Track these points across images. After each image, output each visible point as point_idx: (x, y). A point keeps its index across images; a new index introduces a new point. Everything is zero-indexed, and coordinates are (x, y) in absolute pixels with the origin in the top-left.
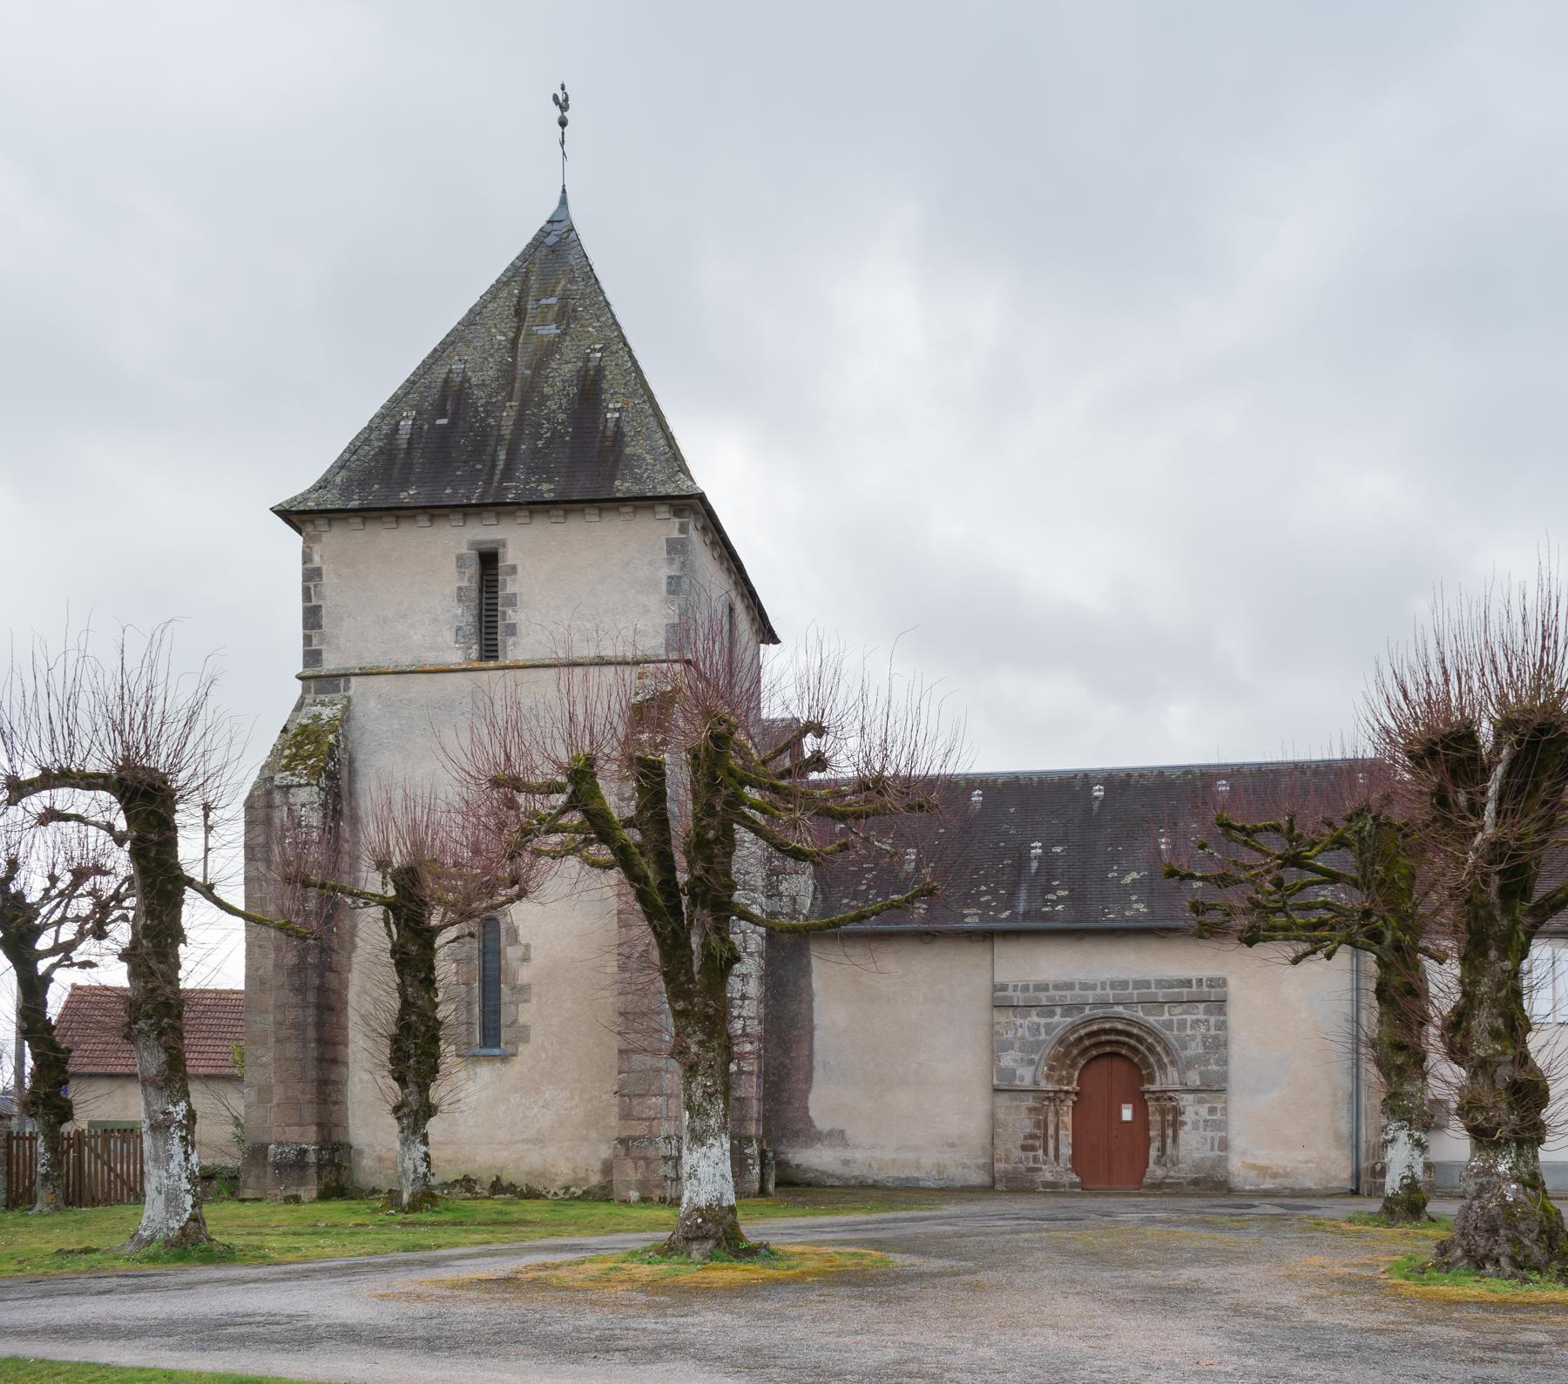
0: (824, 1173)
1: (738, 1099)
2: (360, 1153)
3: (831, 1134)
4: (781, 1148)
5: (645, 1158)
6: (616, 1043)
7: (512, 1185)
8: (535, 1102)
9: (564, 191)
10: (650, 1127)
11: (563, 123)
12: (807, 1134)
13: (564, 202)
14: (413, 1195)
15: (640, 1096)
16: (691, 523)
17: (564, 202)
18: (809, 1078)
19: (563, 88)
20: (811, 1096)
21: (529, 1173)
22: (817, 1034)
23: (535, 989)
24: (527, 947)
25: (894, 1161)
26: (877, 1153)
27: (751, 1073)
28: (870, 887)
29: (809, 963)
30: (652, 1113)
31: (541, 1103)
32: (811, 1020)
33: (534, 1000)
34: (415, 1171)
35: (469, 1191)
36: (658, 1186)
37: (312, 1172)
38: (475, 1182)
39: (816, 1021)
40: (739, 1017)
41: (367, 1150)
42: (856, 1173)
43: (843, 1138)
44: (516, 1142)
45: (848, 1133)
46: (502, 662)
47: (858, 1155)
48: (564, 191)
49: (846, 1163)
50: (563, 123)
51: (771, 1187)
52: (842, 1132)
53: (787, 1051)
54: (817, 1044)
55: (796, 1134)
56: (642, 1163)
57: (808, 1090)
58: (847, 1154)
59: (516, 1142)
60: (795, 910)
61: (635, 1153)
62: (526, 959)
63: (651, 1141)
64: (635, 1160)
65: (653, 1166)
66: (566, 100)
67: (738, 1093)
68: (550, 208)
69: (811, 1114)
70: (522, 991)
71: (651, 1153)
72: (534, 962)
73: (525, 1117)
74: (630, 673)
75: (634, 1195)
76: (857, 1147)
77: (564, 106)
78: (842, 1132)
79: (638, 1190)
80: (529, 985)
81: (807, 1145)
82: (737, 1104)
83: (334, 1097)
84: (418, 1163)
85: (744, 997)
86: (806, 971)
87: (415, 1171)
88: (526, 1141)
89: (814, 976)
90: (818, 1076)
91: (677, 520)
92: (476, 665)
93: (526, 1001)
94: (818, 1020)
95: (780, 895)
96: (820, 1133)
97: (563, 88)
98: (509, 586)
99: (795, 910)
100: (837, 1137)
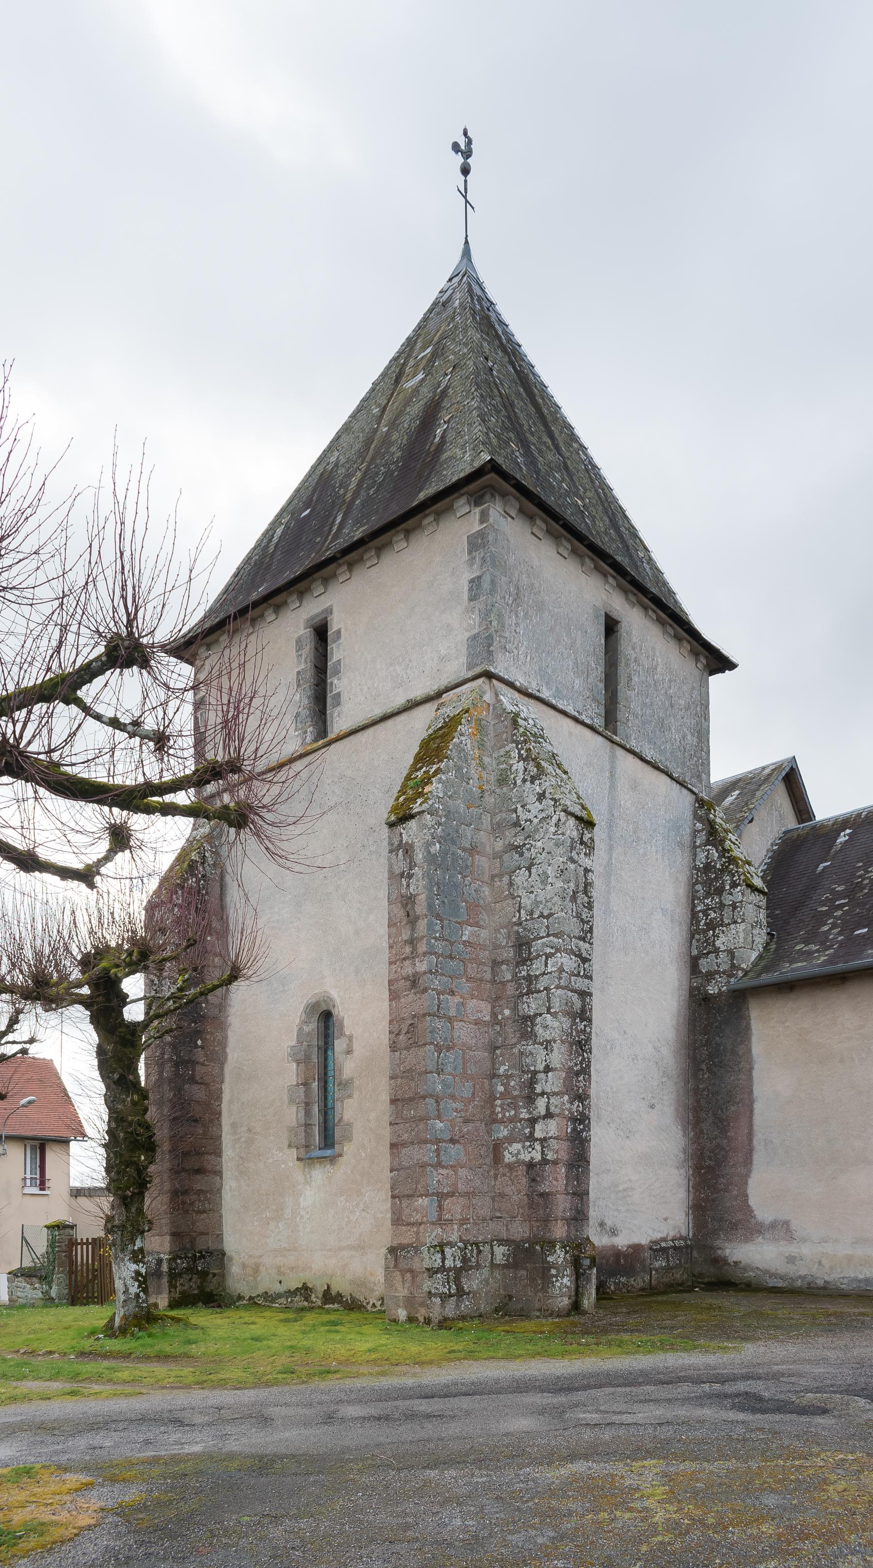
0: (766, 1272)
1: (542, 1195)
2: (231, 1259)
3: (773, 1225)
4: (718, 1243)
5: (411, 1271)
6: (386, 1134)
7: (339, 1295)
8: (357, 1205)
9: (467, 242)
10: (417, 1233)
11: (465, 171)
12: (745, 1226)
13: (467, 253)
14: (125, 1317)
15: (409, 1196)
16: (495, 510)
17: (467, 253)
18: (748, 1161)
19: (465, 133)
20: (751, 1182)
21: (352, 1282)
22: (758, 1106)
23: (357, 1083)
24: (350, 1038)
25: (849, 1258)
26: (829, 1248)
27: (555, 1163)
28: (834, 926)
29: (748, 1027)
30: (418, 1217)
31: (362, 1206)
32: (751, 1092)
33: (356, 1095)
34: (126, 1292)
35: (306, 1299)
36: (422, 1304)
37: (165, 1280)
38: (311, 1290)
39: (756, 1093)
40: (543, 1094)
41: (235, 1256)
42: (803, 1272)
43: (788, 1230)
44: (342, 1249)
45: (794, 1225)
46: (331, 736)
47: (806, 1250)
48: (467, 242)
49: (791, 1260)
50: (465, 171)
51: (589, 1300)
52: (787, 1223)
53: (724, 1131)
54: (757, 1120)
55: (734, 1226)
56: (408, 1275)
57: (747, 1175)
58: (793, 1249)
59: (342, 1249)
60: (733, 966)
61: (403, 1265)
62: (349, 1052)
63: (417, 1249)
64: (403, 1272)
65: (418, 1280)
66: (469, 142)
67: (544, 1188)
68: (452, 261)
69: (752, 1202)
70: (346, 1084)
71: (416, 1265)
72: (355, 1054)
73: (349, 1222)
74: (430, 707)
75: (402, 1314)
76: (804, 1240)
77: (467, 154)
78: (787, 1223)
79: (406, 1308)
80: (352, 1079)
81: (747, 1240)
82: (541, 1201)
83: (198, 1205)
84: (129, 1282)
85: (547, 1069)
86: (744, 1034)
87: (126, 1292)
88: (350, 1247)
89: (754, 1039)
90: (758, 1158)
91: (477, 510)
92: (315, 745)
93: (350, 1096)
94: (758, 1090)
95: (717, 951)
96: (761, 1225)
97: (465, 133)
98: (337, 653)
99: (733, 966)
100: (781, 1229)
